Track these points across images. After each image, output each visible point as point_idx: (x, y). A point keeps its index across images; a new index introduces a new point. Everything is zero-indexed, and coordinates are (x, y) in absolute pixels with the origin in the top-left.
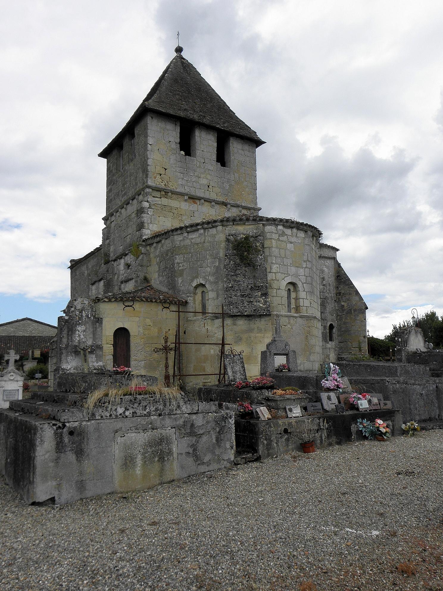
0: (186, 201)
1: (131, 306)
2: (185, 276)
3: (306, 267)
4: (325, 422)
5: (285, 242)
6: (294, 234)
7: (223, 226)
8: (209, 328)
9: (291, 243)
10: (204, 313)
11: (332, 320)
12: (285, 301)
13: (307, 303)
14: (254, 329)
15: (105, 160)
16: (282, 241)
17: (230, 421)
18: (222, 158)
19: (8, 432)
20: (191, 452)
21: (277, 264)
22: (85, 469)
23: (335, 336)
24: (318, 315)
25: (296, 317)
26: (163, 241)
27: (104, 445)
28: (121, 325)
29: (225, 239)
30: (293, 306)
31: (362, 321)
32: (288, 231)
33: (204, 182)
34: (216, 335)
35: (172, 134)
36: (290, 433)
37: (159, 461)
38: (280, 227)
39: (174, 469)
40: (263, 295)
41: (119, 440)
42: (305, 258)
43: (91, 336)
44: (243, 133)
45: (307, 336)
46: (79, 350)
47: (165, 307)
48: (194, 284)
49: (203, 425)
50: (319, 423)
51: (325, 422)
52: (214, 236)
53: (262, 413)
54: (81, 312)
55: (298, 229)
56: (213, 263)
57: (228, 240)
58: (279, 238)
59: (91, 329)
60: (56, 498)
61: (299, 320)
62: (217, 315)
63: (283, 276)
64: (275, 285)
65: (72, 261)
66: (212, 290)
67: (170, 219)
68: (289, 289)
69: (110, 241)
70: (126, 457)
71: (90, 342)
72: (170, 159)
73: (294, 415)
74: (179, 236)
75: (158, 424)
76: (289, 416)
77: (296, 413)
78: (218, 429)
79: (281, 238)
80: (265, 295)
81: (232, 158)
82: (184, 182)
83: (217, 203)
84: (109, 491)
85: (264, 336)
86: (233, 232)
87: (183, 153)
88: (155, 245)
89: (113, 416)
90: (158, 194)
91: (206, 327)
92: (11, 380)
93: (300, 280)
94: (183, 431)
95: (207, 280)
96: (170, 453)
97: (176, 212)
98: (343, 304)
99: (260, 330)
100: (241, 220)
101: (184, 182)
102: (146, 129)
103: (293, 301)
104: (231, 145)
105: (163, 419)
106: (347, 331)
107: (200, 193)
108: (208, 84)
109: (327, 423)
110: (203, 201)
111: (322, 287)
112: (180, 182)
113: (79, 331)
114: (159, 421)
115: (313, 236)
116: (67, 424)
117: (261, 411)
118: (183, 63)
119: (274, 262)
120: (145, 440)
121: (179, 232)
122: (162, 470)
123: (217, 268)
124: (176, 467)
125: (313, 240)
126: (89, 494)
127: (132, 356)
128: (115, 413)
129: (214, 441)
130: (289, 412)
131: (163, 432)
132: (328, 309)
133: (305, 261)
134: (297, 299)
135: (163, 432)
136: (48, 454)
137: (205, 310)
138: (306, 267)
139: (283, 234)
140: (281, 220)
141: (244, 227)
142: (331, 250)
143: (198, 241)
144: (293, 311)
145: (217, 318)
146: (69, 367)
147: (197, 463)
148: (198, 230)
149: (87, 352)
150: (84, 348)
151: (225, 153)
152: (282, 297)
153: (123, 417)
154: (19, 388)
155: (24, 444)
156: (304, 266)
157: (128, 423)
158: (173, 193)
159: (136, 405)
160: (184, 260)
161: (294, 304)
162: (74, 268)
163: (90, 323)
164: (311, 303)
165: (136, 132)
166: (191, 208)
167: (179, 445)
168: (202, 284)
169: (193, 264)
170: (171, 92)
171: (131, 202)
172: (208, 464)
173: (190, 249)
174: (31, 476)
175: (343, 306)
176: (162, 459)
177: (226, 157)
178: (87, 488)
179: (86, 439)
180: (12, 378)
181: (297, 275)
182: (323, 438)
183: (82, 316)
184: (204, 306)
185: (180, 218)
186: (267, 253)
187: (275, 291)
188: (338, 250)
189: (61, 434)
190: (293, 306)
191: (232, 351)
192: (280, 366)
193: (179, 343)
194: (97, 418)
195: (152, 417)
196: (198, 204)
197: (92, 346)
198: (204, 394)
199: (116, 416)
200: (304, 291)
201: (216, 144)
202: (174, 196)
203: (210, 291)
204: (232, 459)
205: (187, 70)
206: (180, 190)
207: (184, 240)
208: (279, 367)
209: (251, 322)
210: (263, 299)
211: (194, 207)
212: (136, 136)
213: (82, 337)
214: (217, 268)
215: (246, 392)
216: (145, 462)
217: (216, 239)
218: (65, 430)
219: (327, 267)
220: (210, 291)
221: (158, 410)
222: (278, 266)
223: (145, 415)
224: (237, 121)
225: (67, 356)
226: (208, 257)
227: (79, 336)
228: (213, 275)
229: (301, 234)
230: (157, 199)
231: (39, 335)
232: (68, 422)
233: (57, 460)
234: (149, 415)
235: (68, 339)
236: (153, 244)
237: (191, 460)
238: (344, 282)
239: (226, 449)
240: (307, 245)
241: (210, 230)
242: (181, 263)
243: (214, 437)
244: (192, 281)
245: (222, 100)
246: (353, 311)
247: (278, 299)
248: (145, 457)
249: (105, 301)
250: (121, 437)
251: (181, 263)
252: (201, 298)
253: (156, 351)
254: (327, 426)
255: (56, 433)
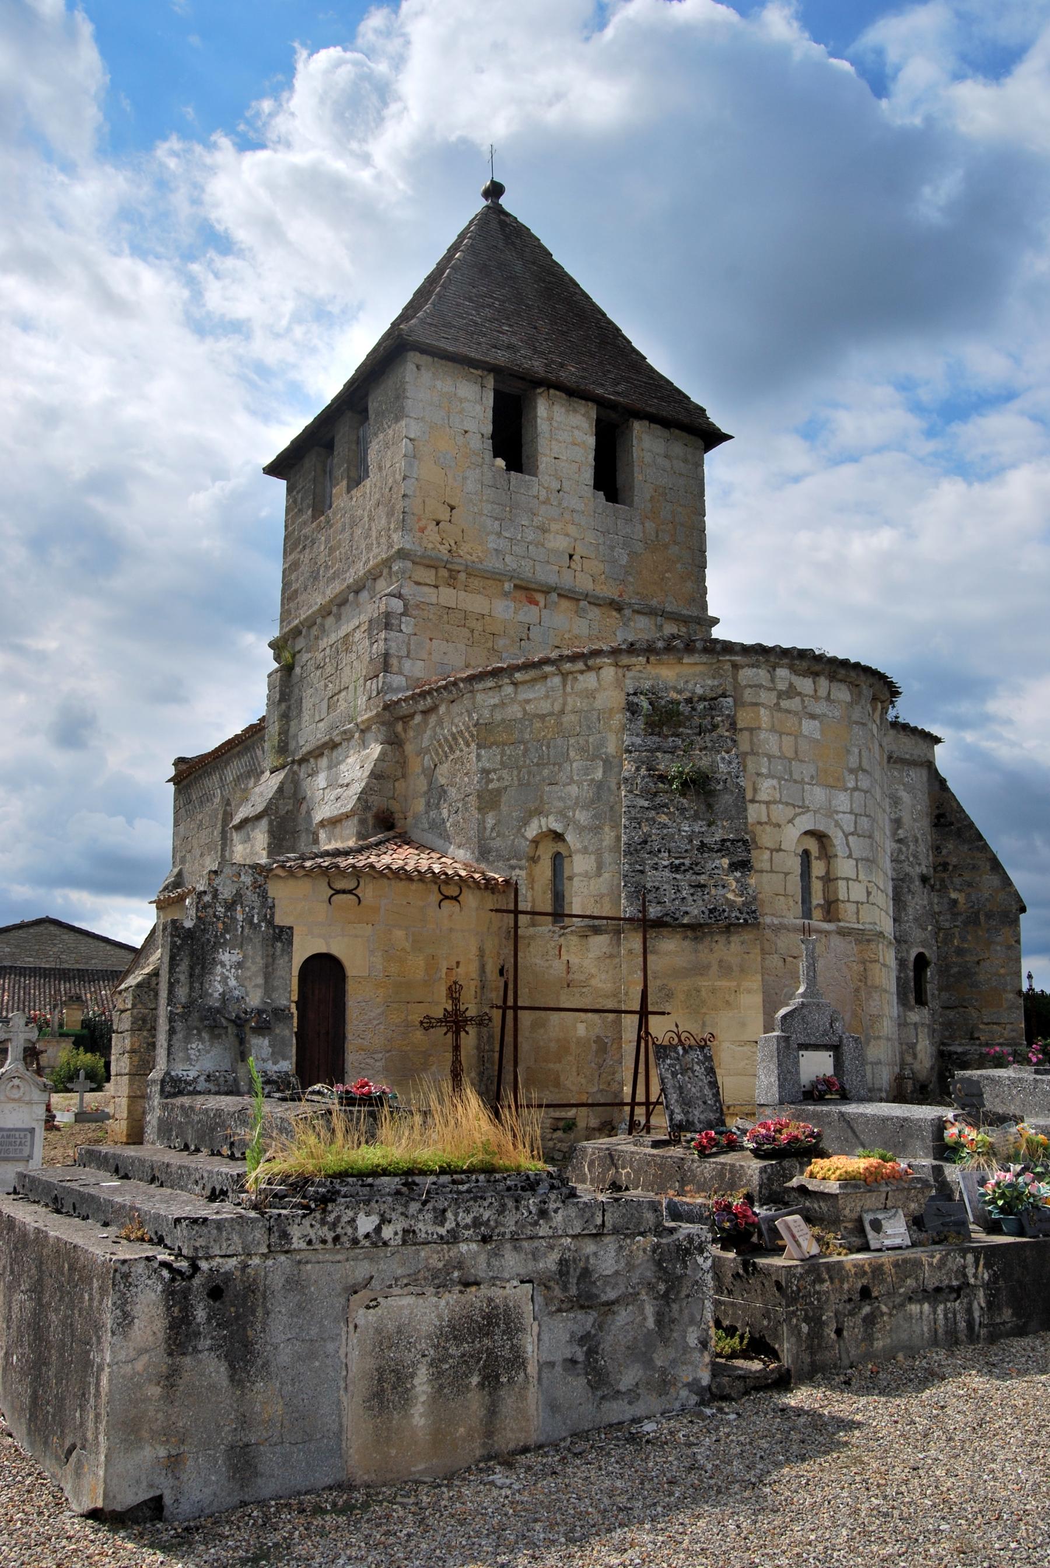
0: (506, 594)
1: (350, 892)
2: (504, 808)
3: (856, 789)
4: (982, 1263)
5: (796, 713)
6: (822, 692)
7: (617, 665)
8: (574, 960)
9: (813, 717)
10: (558, 914)
11: (924, 943)
12: (795, 883)
13: (858, 892)
14: (708, 967)
15: (281, 485)
16: (788, 711)
17: (700, 1260)
18: (609, 478)
19: (12, 1272)
20: (580, 1357)
21: (773, 777)
22: (258, 1408)
23: (931, 988)
24: (887, 926)
25: (827, 933)
26: (442, 709)
27: (314, 1331)
28: (336, 949)
29: (623, 704)
30: (817, 899)
31: (1009, 947)
32: (805, 685)
33: (559, 543)
34: (593, 982)
35: (474, 407)
36: (876, 1298)
37: (481, 1385)
38: (782, 673)
39: (527, 1412)
40: (734, 866)
41: (362, 1317)
42: (853, 761)
43: (260, 980)
44: (667, 411)
45: (857, 990)
46: (224, 1022)
47: (446, 897)
48: (532, 831)
49: (617, 1273)
50: (965, 1267)
51: (982, 1263)
52: (591, 695)
53: (793, 1236)
54: (230, 906)
55: (832, 678)
56: (587, 771)
57: (632, 709)
58: (777, 704)
59: (258, 959)
60: (168, 1500)
61: (836, 941)
62: (597, 922)
63: (790, 812)
64: (766, 838)
65: (180, 761)
66: (585, 851)
67: (462, 646)
68: (806, 853)
69: (289, 707)
70: (380, 1370)
71: (254, 1000)
72: (465, 478)
73: (887, 1242)
74: (491, 693)
75: (480, 1268)
76: (873, 1244)
77: (895, 1235)
78: (662, 1287)
79: (785, 704)
80: (743, 866)
81: (638, 477)
82: (502, 544)
83: (596, 602)
84: (329, 1481)
85: (739, 986)
86: (647, 685)
87: (500, 462)
88: (418, 718)
89: (344, 1239)
90: (429, 576)
91: (564, 957)
92: (14, 1100)
93: (837, 824)
94: (557, 1291)
95: (568, 822)
96: (518, 1361)
97: (478, 626)
98: (954, 895)
99: (725, 969)
100: (669, 649)
101: (502, 544)
102: (400, 396)
103: (817, 886)
104: (635, 442)
105: (496, 1254)
106: (966, 974)
107: (547, 575)
108: (572, 280)
109: (987, 1266)
110: (554, 596)
111: (895, 846)
112: (492, 543)
113: (223, 965)
114: (482, 1258)
115: (875, 699)
116: (204, 1265)
117: (788, 1228)
118: (503, 225)
119: (764, 771)
120: (440, 1317)
121: (490, 683)
122: (492, 1411)
123: (599, 786)
124: (533, 1407)
125: (874, 710)
126: (266, 1487)
127: (349, 1036)
128: (350, 1231)
129: (650, 1323)
130: (871, 1234)
131: (496, 1293)
132: (910, 911)
133: (851, 771)
134: (828, 879)
135: (496, 1293)
136: (145, 1358)
137: (562, 907)
138: (856, 789)
139: (791, 692)
140: (785, 653)
141: (678, 669)
142: (920, 742)
143: (545, 707)
144: (817, 914)
145: (597, 931)
146: (192, 1074)
147: (599, 1393)
148: (545, 677)
149: (247, 1029)
150: (238, 1017)
151: (619, 465)
152: (786, 874)
153: (374, 1245)
154: (34, 1125)
155: (66, 1317)
156: (851, 784)
157: (391, 1266)
158: (471, 572)
159: (414, 1207)
160: (502, 763)
161: (820, 894)
162: (185, 783)
163: (257, 940)
164: (869, 893)
165: (373, 406)
166: (521, 617)
167: (545, 1337)
168: (555, 832)
169: (529, 773)
170: (471, 300)
171: (351, 597)
172: (632, 1395)
173: (521, 732)
174: (90, 1424)
175: (955, 902)
176: (491, 1381)
177: (621, 479)
178: (261, 1468)
179: (260, 1313)
180: (17, 1097)
181: (831, 812)
182: (977, 1314)
183: (234, 919)
184: (558, 897)
185: (490, 644)
186: (745, 747)
187: (766, 855)
188: (937, 740)
189: (186, 1293)
190: (817, 899)
191: (679, 1037)
192: (818, 1081)
193: (516, 1008)
194: (295, 1246)
195: (463, 1247)
196: (542, 604)
197: (260, 1012)
198: (591, 1164)
199: (355, 1242)
200: (850, 856)
201: (591, 441)
202: (476, 583)
203: (578, 851)
204: (705, 1382)
205: (513, 243)
206: (493, 563)
207: (503, 704)
208: (814, 1084)
209: (700, 947)
210: (737, 881)
211: (530, 614)
212: (371, 421)
213: (232, 983)
214: (599, 786)
215: (733, 1166)
216: (441, 1387)
217: (598, 704)
218: (197, 1281)
219: (910, 789)
220: (578, 851)
221: (481, 1224)
222: (775, 782)
223: (441, 1237)
224: (652, 378)
225: (187, 1039)
226: (572, 754)
227: (225, 980)
228: (586, 807)
229: (842, 693)
230: (426, 589)
231: (78, 966)
232: (208, 1258)
233: (170, 1378)
234: (453, 1238)
235: (192, 989)
236: (412, 716)
237: (579, 1383)
238: (959, 834)
239: (686, 1349)
240: (856, 723)
241: (580, 677)
242: (495, 771)
243: (649, 1310)
244: (526, 822)
245: (610, 323)
246: (982, 918)
247: (775, 882)
248: (441, 1373)
249: (277, 876)
250: (368, 1307)
251: (495, 771)
252: (549, 873)
253: (428, 1024)
254: (986, 1276)
255: (169, 1293)
